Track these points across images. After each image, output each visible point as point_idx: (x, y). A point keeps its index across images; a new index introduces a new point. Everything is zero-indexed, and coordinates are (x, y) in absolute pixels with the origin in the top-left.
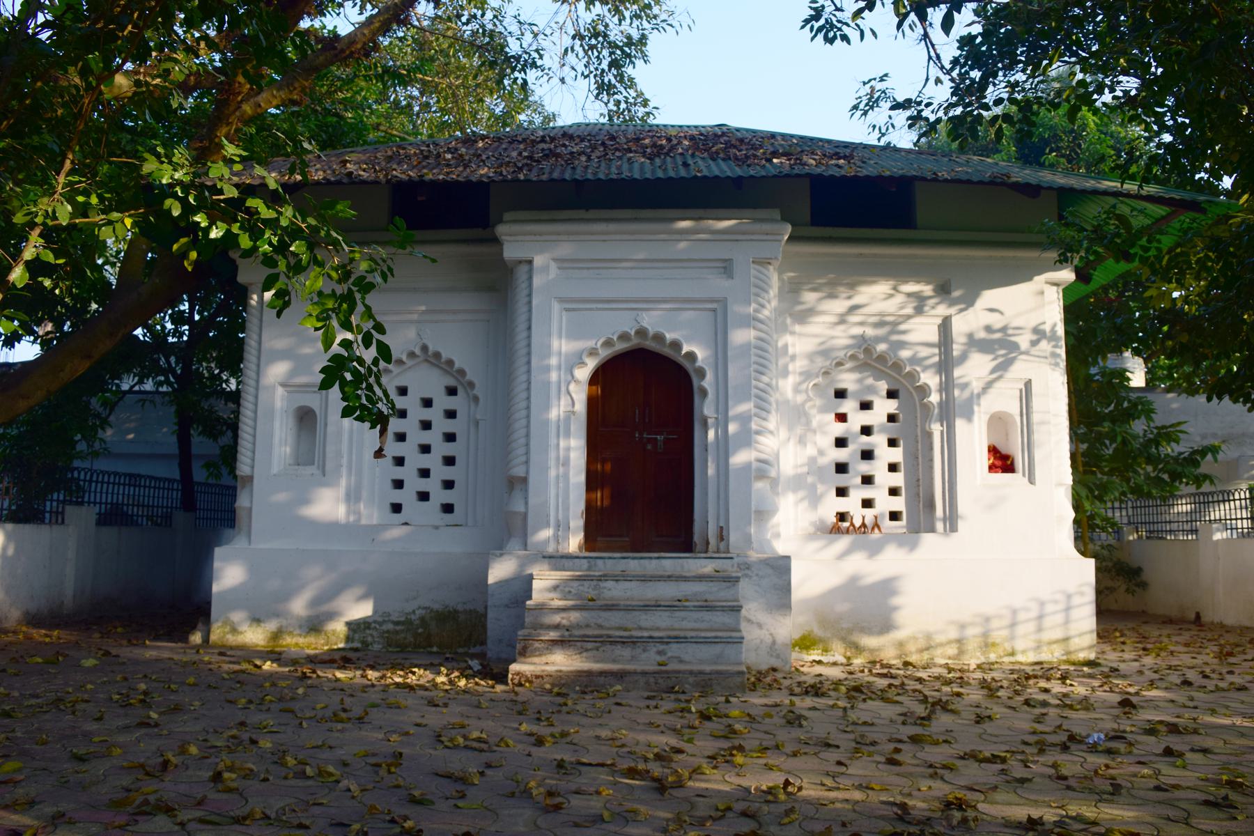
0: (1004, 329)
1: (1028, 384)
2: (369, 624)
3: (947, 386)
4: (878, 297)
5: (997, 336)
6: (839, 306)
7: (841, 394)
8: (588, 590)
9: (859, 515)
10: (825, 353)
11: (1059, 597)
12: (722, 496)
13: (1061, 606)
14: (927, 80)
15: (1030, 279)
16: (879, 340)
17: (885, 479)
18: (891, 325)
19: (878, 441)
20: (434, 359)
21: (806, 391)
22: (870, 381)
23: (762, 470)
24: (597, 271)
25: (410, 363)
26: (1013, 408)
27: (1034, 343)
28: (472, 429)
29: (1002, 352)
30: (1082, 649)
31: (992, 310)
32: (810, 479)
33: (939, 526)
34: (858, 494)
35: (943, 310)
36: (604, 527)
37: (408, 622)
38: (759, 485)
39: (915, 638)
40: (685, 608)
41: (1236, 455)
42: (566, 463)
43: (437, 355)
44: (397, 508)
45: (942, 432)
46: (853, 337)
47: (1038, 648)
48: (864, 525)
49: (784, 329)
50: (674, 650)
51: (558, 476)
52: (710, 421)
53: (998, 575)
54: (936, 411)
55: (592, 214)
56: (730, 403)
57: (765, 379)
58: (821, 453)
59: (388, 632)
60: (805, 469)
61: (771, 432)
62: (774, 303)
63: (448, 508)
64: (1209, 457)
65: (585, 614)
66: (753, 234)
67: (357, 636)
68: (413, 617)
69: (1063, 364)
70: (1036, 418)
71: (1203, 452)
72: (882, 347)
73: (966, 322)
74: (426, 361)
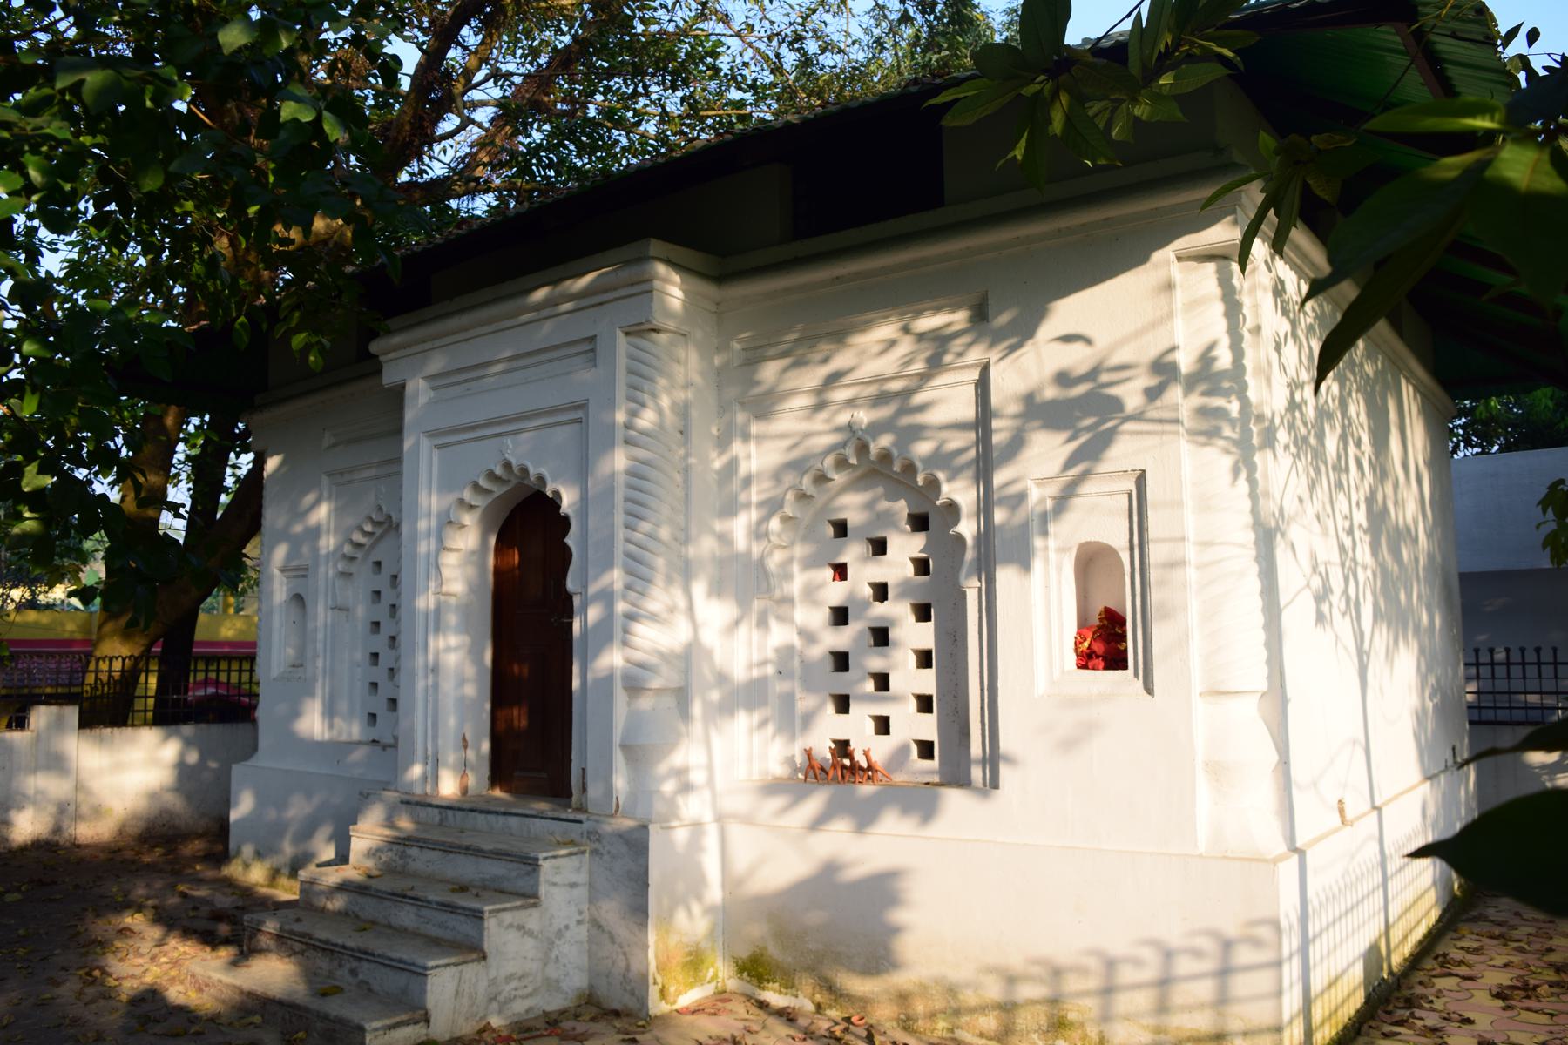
4: (878, 350)
6: (812, 377)
9: (868, 745)
10: (797, 465)
13: (1208, 965)
16: (876, 428)
18: (898, 400)
24: (467, 385)
26: (1116, 535)
29: (1088, 422)
31: (1068, 339)
32: (781, 687)
35: (976, 355)
39: (924, 989)
46: (838, 429)
56: (591, 572)
57: (645, 526)
58: (808, 636)
70: (1156, 553)
72: (885, 441)
73: (1021, 372)
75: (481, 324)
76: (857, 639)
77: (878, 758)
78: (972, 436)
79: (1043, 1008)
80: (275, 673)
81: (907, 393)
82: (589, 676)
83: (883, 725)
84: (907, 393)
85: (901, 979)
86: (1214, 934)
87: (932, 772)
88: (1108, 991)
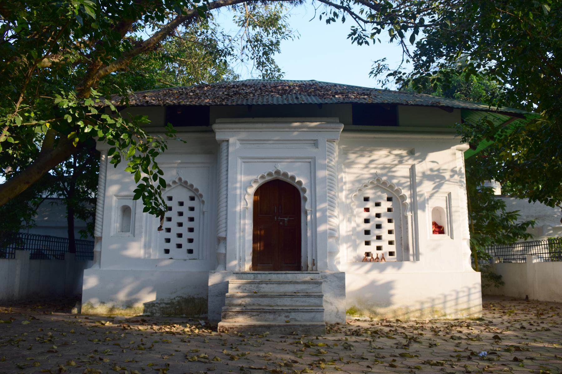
0: (438, 170)
1: (450, 194)
2: (154, 304)
3: (414, 196)
4: (383, 156)
5: (436, 173)
6: (365, 160)
7: (366, 199)
8: (253, 288)
9: (375, 253)
10: (359, 181)
11: (465, 289)
12: (314, 246)
13: (466, 294)
14: (403, 60)
15: (449, 148)
16: (383, 175)
17: (387, 237)
18: (388, 168)
23: (332, 233)
25: (173, 186)
26: (443, 204)
27: (452, 176)
28: (201, 216)
29: (438, 180)
30: (476, 313)
31: (433, 162)
32: (353, 237)
34: (375, 244)
35: (411, 162)
36: (261, 260)
37: (172, 303)
38: (330, 240)
39: (401, 309)
40: (298, 296)
42: (244, 230)
43: (186, 182)
44: (167, 251)
45: (412, 216)
46: (372, 174)
47: (456, 312)
49: (341, 171)
50: (293, 315)
51: (240, 237)
53: (439, 280)
54: (409, 206)
55: (256, 119)
57: (333, 193)
58: (358, 225)
59: (163, 308)
60: (351, 233)
61: (336, 217)
63: (190, 251)
66: (327, 128)
67: (148, 310)
68: (174, 301)
69: (465, 186)
70: (453, 209)
71: (528, 224)
72: (384, 178)
73: (422, 167)
74: (181, 185)
75: (266, 128)
77: (380, 256)
79: (419, 312)
80: (112, 234)
81: (390, 168)
84: (390, 168)
86: (467, 287)
87: (394, 259)
88: (445, 302)
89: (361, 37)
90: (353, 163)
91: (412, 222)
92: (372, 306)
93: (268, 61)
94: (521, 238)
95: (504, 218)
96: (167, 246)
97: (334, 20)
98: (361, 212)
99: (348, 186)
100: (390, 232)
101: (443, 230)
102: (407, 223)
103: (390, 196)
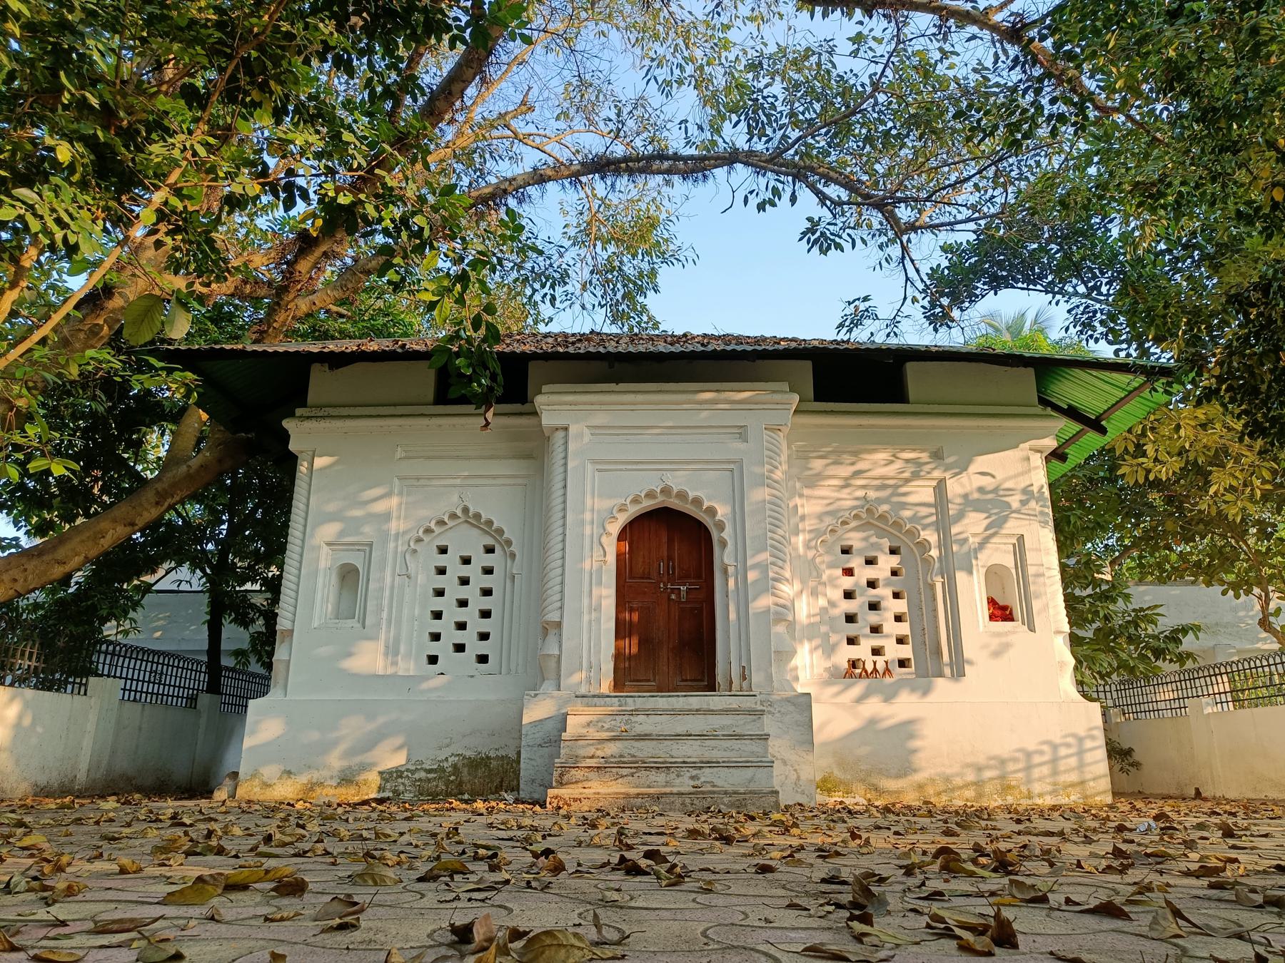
0: (995, 490)
3: (945, 542)
4: (880, 463)
5: (990, 496)
6: (846, 471)
7: (846, 551)
8: (620, 723)
14: (905, 298)
16: (880, 501)
17: (891, 628)
18: (894, 487)
19: (884, 592)
20: (474, 520)
21: (816, 547)
22: (874, 539)
23: (782, 613)
25: (451, 523)
26: (1009, 561)
27: (1024, 503)
28: (508, 581)
30: (1099, 794)
33: (947, 671)
34: (867, 644)
35: (937, 474)
36: (629, 673)
38: (780, 629)
39: (932, 780)
40: (715, 738)
41: (1211, 644)
42: (598, 608)
43: (478, 516)
45: (943, 583)
47: (1054, 792)
48: (875, 670)
49: (794, 493)
50: (706, 775)
51: (590, 622)
52: (731, 570)
53: (1011, 713)
54: (937, 565)
58: (832, 604)
59: (420, 780)
60: (818, 619)
61: (787, 580)
62: (785, 467)
63: (483, 659)
64: (1191, 635)
65: (618, 744)
68: (445, 765)
69: (1051, 523)
70: (1031, 570)
71: (1184, 630)
72: (885, 507)
74: (467, 522)
76: (861, 606)
78: (933, 510)
82: (751, 612)
83: (876, 652)
85: (919, 777)
89: (826, 239)
90: (820, 476)
91: (944, 596)
92: (869, 773)
93: (635, 310)
94: (1171, 661)
95: (1128, 622)
96: (434, 648)
97: (774, 205)
98: (838, 578)
99: (808, 525)
100: (898, 618)
101: (1011, 613)
102: (935, 599)
103: (895, 544)
